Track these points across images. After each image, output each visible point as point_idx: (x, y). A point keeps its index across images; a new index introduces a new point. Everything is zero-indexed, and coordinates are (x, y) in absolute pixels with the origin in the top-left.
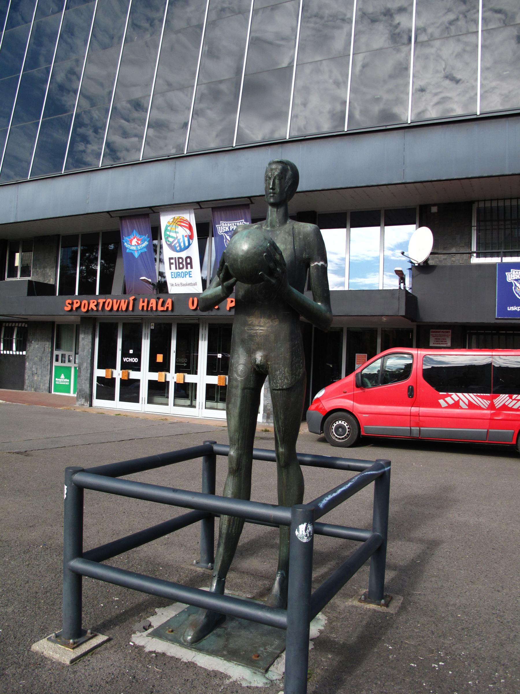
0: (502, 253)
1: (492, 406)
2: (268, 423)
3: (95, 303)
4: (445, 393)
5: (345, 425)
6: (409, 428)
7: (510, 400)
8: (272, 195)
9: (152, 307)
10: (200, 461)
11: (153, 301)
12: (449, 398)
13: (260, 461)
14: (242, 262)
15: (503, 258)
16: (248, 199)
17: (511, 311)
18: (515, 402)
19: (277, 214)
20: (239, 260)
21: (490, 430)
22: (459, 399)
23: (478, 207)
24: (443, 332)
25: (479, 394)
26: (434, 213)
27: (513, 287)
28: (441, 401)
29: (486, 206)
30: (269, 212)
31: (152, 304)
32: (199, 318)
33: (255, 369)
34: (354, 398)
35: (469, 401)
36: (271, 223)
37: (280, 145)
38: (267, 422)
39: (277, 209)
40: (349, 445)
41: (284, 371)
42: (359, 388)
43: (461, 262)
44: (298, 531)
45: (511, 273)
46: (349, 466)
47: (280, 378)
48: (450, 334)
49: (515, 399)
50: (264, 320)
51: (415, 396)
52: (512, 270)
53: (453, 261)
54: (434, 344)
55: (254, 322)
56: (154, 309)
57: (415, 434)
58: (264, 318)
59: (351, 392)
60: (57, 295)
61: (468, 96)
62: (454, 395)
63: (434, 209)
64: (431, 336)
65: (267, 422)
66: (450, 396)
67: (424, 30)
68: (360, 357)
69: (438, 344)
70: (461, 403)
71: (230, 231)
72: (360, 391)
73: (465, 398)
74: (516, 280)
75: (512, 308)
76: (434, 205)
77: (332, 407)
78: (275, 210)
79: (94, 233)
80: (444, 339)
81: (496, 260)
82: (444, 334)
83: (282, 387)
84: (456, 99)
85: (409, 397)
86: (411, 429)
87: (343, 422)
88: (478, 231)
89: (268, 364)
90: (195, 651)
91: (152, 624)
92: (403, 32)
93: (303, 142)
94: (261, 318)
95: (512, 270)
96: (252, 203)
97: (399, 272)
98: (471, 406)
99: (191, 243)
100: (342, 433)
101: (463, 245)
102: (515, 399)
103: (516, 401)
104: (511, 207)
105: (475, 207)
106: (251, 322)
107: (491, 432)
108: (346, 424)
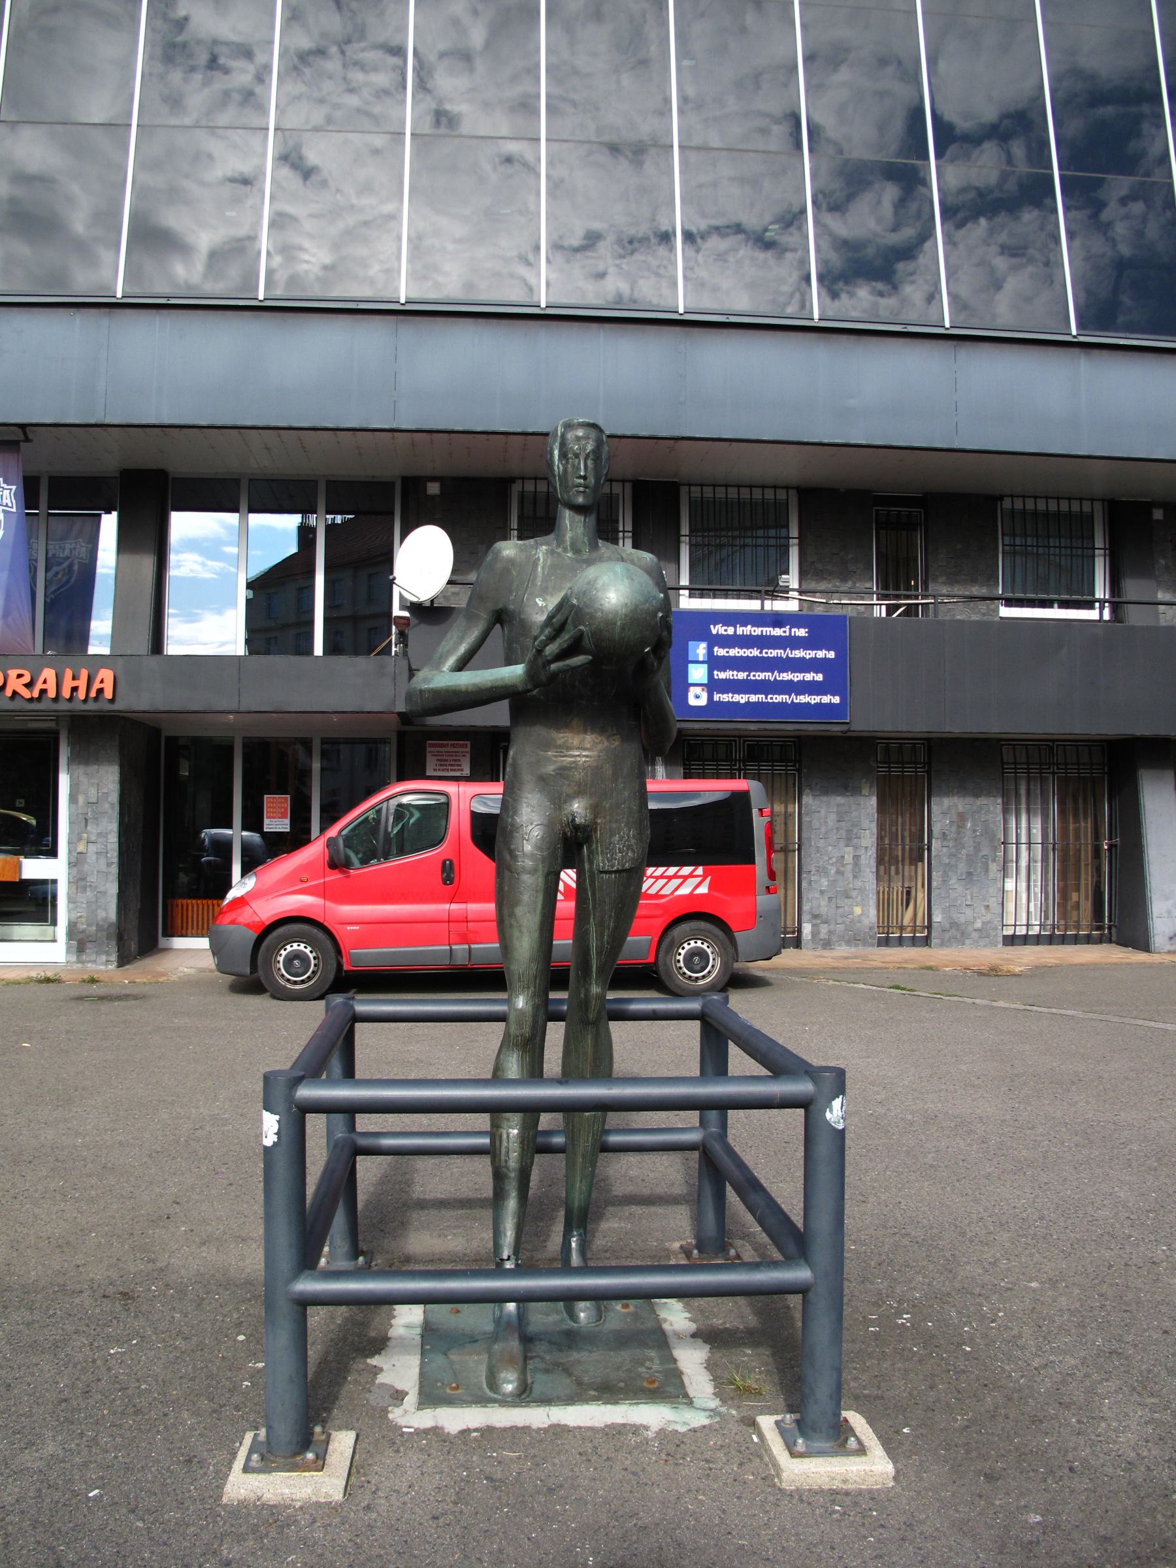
2: (83, 962)
3: (27, 679)
5: (308, 951)
6: (448, 947)
8: (581, 489)
9: (100, 691)
11: (49, 674)
13: (443, 1024)
14: (623, 628)
16: (19, 431)
18: (662, 882)
19: (584, 527)
20: (619, 623)
26: (433, 497)
30: (567, 522)
31: (102, 682)
32: (57, 716)
33: (565, 834)
34: (323, 892)
36: (573, 544)
37: (107, 310)
38: (79, 961)
39: (585, 517)
40: (317, 994)
41: (628, 836)
42: (336, 871)
44: (831, 1111)
46: (654, 1011)
47: (619, 849)
48: (468, 749)
49: (651, 877)
50: (593, 736)
54: (435, 770)
55: (571, 741)
56: (108, 694)
57: (461, 959)
58: (592, 733)
59: (318, 878)
60: (318, 649)
61: (341, 225)
63: (433, 488)
65: (79, 961)
67: (382, 93)
68: (273, 803)
69: (443, 770)
72: (340, 876)
76: (433, 479)
77: (276, 915)
78: (582, 518)
82: (455, 750)
83: (623, 866)
84: (308, 225)
85: (446, 884)
86: (470, 948)
87: (302, 945)
89: (596, 823)
90: (538, 1406)
91: (399, 1387)
92: (199, 42)
93: (165, 312)
94: (585, 733)
96: (27, 440)
97: (402, 621)
99: (530, 1381)
100: (300, 971)
102: (651, 877)
105: (516, 488)
106: (562, 740)
108: (309, 949)
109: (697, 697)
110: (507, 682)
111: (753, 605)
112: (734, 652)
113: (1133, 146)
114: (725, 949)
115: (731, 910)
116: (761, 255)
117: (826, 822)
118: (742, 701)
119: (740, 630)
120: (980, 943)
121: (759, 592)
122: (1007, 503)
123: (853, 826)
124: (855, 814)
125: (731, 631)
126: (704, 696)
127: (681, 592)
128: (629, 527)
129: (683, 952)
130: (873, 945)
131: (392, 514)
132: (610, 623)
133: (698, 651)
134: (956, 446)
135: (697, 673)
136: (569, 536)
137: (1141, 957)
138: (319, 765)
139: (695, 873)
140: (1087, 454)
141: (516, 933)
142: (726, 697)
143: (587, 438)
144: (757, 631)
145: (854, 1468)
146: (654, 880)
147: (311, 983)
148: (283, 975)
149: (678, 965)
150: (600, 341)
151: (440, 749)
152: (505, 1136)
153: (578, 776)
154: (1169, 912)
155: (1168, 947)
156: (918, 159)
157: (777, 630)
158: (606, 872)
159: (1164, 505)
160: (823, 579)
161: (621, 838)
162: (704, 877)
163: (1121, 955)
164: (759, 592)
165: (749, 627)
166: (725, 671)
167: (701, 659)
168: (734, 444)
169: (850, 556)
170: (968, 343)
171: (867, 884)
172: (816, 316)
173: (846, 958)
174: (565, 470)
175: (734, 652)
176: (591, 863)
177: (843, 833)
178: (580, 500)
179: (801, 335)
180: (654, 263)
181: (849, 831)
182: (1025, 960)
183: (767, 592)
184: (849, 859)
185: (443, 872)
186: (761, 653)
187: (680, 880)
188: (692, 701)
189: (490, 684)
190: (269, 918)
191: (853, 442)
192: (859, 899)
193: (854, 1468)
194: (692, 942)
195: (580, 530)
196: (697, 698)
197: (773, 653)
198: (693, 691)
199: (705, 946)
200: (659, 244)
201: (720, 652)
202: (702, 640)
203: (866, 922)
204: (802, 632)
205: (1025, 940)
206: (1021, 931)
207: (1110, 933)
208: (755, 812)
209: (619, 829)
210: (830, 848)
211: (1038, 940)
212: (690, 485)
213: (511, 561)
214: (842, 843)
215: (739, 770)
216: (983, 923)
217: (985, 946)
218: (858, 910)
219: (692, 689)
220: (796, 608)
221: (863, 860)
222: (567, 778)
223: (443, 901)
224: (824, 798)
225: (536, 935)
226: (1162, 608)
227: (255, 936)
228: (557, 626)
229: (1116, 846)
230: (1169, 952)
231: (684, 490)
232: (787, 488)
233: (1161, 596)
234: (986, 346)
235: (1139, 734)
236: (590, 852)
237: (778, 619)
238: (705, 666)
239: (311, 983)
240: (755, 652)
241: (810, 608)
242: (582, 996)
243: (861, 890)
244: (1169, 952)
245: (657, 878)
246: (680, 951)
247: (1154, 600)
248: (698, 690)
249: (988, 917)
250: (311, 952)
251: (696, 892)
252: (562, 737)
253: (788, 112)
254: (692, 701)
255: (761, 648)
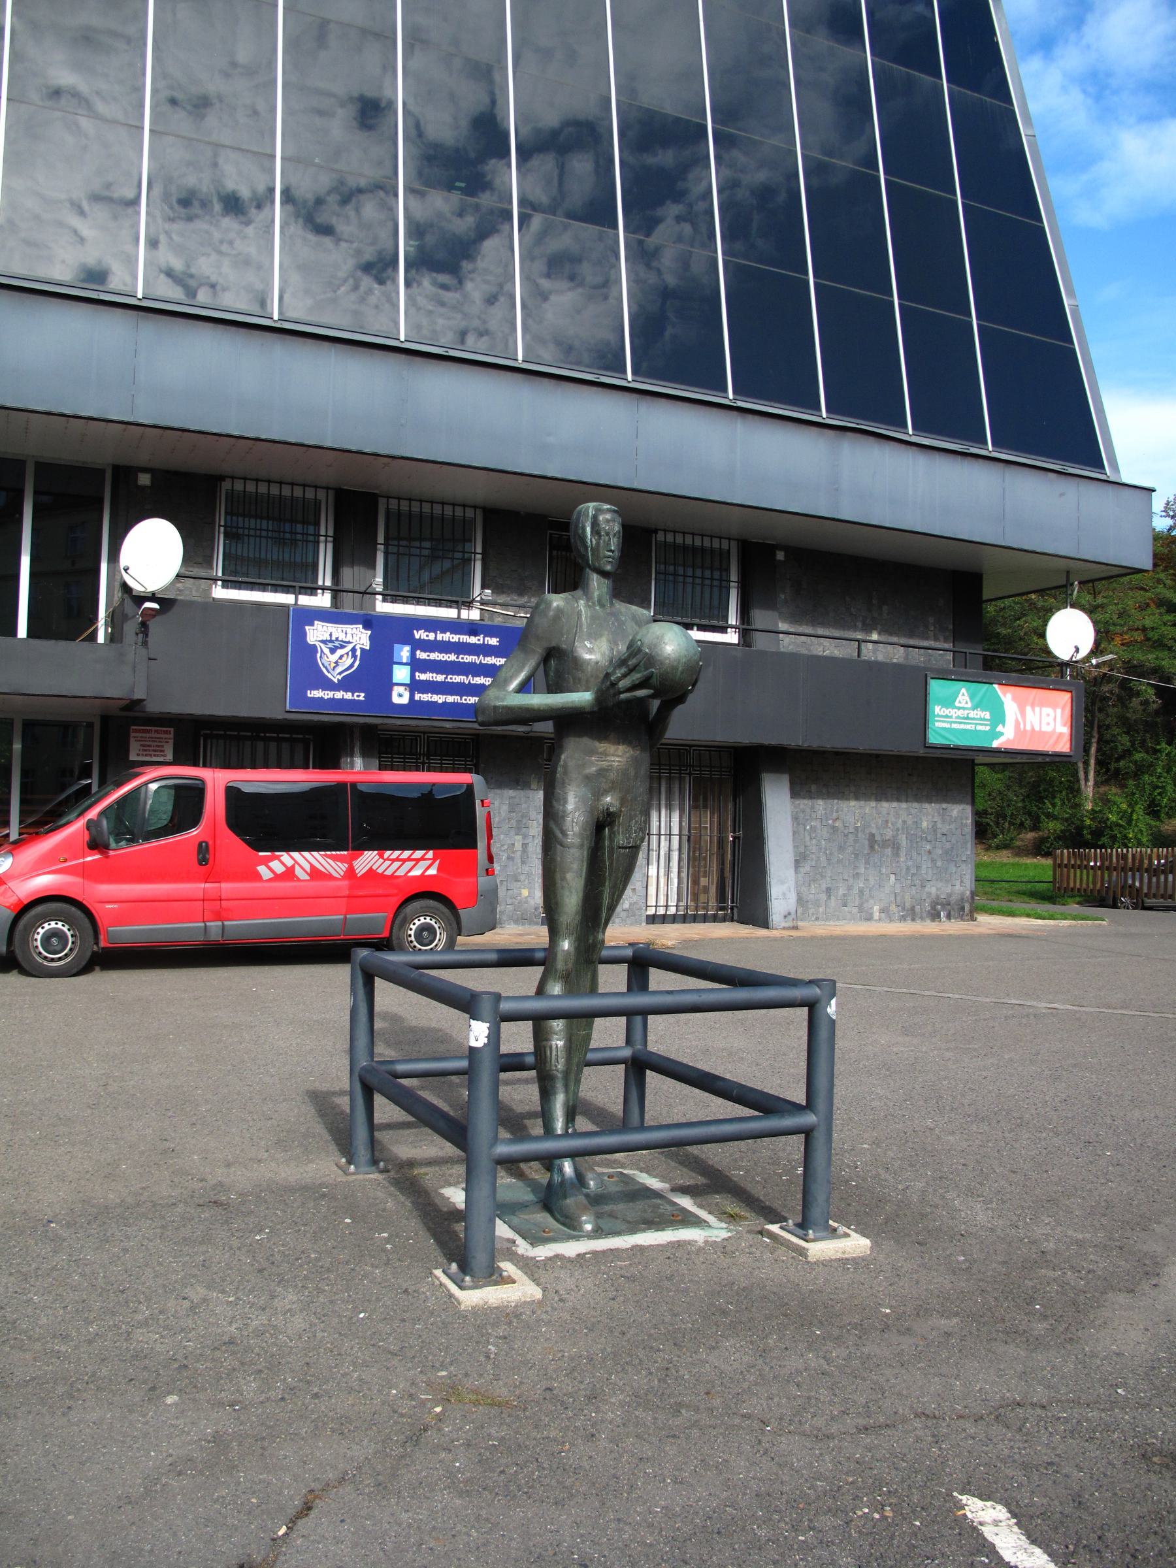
0: (297, 589)
1: (351, 872)
4: (269, 854)
5: (65, 929)
6: (202, 924)
7: (381, 861)
10: (806, 1009)
12: (276, 861)
14: (682, 673)
15: (300, 597)
17: (313, 699)
18: (397, 864)
21: (348, 916)
22: (293, 862)
23: (388, 508)
24: (157, 731)
25: (328, 853)
26: (144, 488)
27: (319, 655)
28: (262, 869)
29: (467, 515)
34: (84, 872)
35: (311, 865)
36: (599, 601)
43: (194, 593)
45: (315, 627)
48: (172, 736)
49: (388, 859)
51: (211, 862)
52: (316, 622)
53: (180, 591)
54: (138, 755)
60: (22, 631)
62: (285, 857)
63: (144, 479)
64: (132, 741)
66: (278, 858)
69: (146, 755)
70: (298, 872)
71: (331, 641)
72: (99, 856)
73: (303, 861)
74: (323, 642)
75: (316, 692)
76: (145, 470)
79: (60, 465)
80: (159, 746)
81: (287, 599)
85: (202, 865)
86: (206, 926)
87: (60, 924)
88: (386, 554)
89: (621, 811)
94: (619, 744)
95: (316, 622)
98: (315, 874)
100: (58, 948)
101: (200, 560)
102: (388, 859)
103: (413, 863)
104: (292, 500)
105: (226, 485)
107: (350, 919)
109: (400, 695)
110: (577, 704)
111: (450, 613)
112: (435, 656)
113: (680, 185)
114: (450, 925)
115: (455, 893)
116: (312, 237)
117: (499, 813)
118: (440, 701)
119: (440, 637)
120: (628, 922)
121: (457, 602)
122: (660, 536)
123: (523, 816)
124: (524, 806)
125: (432, 636)
126: (407, 695)
127: (378, 597)
128: (331, 533)
129: (414, 927)
130: (537, 924)
131: (101, 501)
132: (675, 668)
133: (402, 654)
134: (635, 486)
135: (401, 674)
136: (596, 594)
137: (762, 932)
138: (20, 746)
139: (426, 857)
140: (739, 502)
141: (567, 893)
142: (426, 697)
143: (613, 520)
144: (455, 638)
145: (849, 1244)
146: (390, 862)
147: (69, 959)
148: (40, 953)
149: (410, 939)
150: (332, 358)
151: (144, 735)
152: (554, 1047)
153: (612, 776)
154: (784, 894)
155: (783, 925)
156: (608, 227)
157: (473, 637)
158: (623, 848)
159: (786, 548)
160: (503, 593)
161: (636, 822)
162: (434, 860)
163: (747, 931)
164: (457, 602)
165: (448, 633)
166: (425, 673)
167: (405, 661)
168: (445, 467)
169: (527, 573)
170: (648, 398)
171: (533, 870)
172: (520, 357)
173: (520, 935)
174: (598, 544)
175: (435, 656)
176: (611, 840)
177: (514, 822)
178: (608, 568)
179: (509, 374)
180: (217, 235)
181: (519, 822)
182: (672, 935)
183: (464, 603)
184: (518, 846)
185: (198, 854)
186: (458, 658)
187: (413, 863)
188: (396, 699)
189: (561, 705)
190: (27, 897)
191: (550, 475)
192: (526, 882)
193: (849, 1244)
194: (422, 918)
195: (605, 590)
196: (400, 697)
197: (469, 659)
198: (396, 690)
199: (433, 922)
200: (223, 216)
201: (421, 655)
202: (406, 643)
203: (532, 902)
204: (494, 641)
205: (664, 919)
206: (661, 911)
207: (732, 913)
208: (478, 802)
209: (636, 816)
210: (502, 836)
211: (674, 919)
212: (388, 497)
213: (559, 611)
214: (513, 832)
215: (423, 763)
216: (631, 904)
217: (631, 924)
218: (525, 893)
219: (396, 688)
220: (478, 618)
221: (530, 848)
222: (604, 777)
223: (201, 882)
224: (498, 791)
225: (581, 895)
226: (781, 635)
227: (13, 914)
228: (631, 667)
229: (739, 838)
230: (784, 928)
231: (382, 503)
232: (475, 507)
233: (782, 626)
234: (663, 401)
235: (766, 743)
236: (612, 833)
237: (472, 628)
238: (409, 668)
239: (69, 959)
240: (452, 657)
241: (491, 619)
242: (591, 941)
243: (529, 875)
244: (784, 928)
245: (393, 860)
246: (412, 926)
247: (775, 630)
248: (401, 689)
249: (635, 899)
250: (69, 930)
251: (426, 873)
252: (602, 746)
253: (355, 94)
254: (396, 699)
255: (458, 653)
